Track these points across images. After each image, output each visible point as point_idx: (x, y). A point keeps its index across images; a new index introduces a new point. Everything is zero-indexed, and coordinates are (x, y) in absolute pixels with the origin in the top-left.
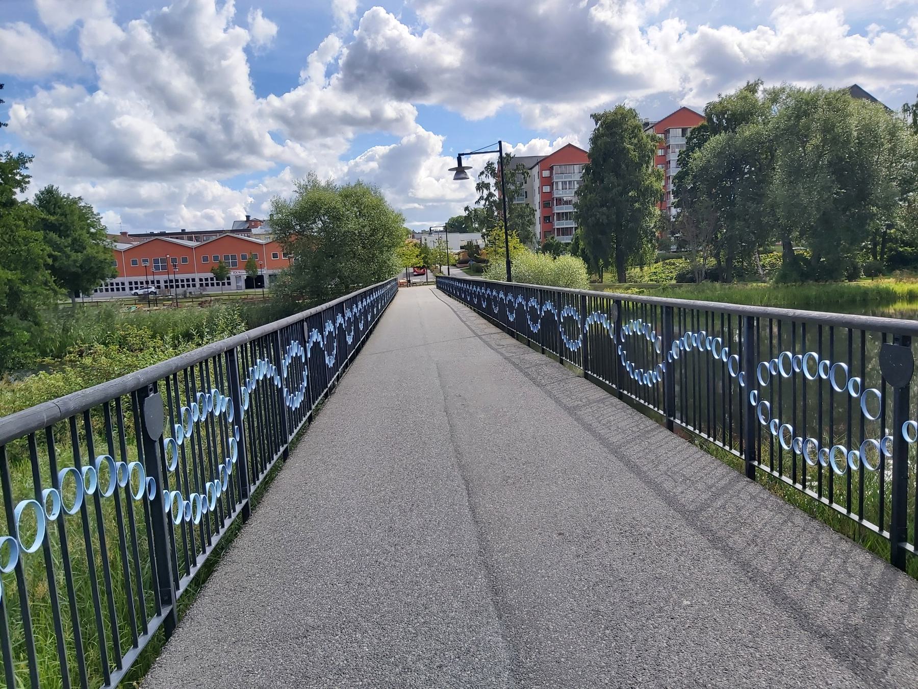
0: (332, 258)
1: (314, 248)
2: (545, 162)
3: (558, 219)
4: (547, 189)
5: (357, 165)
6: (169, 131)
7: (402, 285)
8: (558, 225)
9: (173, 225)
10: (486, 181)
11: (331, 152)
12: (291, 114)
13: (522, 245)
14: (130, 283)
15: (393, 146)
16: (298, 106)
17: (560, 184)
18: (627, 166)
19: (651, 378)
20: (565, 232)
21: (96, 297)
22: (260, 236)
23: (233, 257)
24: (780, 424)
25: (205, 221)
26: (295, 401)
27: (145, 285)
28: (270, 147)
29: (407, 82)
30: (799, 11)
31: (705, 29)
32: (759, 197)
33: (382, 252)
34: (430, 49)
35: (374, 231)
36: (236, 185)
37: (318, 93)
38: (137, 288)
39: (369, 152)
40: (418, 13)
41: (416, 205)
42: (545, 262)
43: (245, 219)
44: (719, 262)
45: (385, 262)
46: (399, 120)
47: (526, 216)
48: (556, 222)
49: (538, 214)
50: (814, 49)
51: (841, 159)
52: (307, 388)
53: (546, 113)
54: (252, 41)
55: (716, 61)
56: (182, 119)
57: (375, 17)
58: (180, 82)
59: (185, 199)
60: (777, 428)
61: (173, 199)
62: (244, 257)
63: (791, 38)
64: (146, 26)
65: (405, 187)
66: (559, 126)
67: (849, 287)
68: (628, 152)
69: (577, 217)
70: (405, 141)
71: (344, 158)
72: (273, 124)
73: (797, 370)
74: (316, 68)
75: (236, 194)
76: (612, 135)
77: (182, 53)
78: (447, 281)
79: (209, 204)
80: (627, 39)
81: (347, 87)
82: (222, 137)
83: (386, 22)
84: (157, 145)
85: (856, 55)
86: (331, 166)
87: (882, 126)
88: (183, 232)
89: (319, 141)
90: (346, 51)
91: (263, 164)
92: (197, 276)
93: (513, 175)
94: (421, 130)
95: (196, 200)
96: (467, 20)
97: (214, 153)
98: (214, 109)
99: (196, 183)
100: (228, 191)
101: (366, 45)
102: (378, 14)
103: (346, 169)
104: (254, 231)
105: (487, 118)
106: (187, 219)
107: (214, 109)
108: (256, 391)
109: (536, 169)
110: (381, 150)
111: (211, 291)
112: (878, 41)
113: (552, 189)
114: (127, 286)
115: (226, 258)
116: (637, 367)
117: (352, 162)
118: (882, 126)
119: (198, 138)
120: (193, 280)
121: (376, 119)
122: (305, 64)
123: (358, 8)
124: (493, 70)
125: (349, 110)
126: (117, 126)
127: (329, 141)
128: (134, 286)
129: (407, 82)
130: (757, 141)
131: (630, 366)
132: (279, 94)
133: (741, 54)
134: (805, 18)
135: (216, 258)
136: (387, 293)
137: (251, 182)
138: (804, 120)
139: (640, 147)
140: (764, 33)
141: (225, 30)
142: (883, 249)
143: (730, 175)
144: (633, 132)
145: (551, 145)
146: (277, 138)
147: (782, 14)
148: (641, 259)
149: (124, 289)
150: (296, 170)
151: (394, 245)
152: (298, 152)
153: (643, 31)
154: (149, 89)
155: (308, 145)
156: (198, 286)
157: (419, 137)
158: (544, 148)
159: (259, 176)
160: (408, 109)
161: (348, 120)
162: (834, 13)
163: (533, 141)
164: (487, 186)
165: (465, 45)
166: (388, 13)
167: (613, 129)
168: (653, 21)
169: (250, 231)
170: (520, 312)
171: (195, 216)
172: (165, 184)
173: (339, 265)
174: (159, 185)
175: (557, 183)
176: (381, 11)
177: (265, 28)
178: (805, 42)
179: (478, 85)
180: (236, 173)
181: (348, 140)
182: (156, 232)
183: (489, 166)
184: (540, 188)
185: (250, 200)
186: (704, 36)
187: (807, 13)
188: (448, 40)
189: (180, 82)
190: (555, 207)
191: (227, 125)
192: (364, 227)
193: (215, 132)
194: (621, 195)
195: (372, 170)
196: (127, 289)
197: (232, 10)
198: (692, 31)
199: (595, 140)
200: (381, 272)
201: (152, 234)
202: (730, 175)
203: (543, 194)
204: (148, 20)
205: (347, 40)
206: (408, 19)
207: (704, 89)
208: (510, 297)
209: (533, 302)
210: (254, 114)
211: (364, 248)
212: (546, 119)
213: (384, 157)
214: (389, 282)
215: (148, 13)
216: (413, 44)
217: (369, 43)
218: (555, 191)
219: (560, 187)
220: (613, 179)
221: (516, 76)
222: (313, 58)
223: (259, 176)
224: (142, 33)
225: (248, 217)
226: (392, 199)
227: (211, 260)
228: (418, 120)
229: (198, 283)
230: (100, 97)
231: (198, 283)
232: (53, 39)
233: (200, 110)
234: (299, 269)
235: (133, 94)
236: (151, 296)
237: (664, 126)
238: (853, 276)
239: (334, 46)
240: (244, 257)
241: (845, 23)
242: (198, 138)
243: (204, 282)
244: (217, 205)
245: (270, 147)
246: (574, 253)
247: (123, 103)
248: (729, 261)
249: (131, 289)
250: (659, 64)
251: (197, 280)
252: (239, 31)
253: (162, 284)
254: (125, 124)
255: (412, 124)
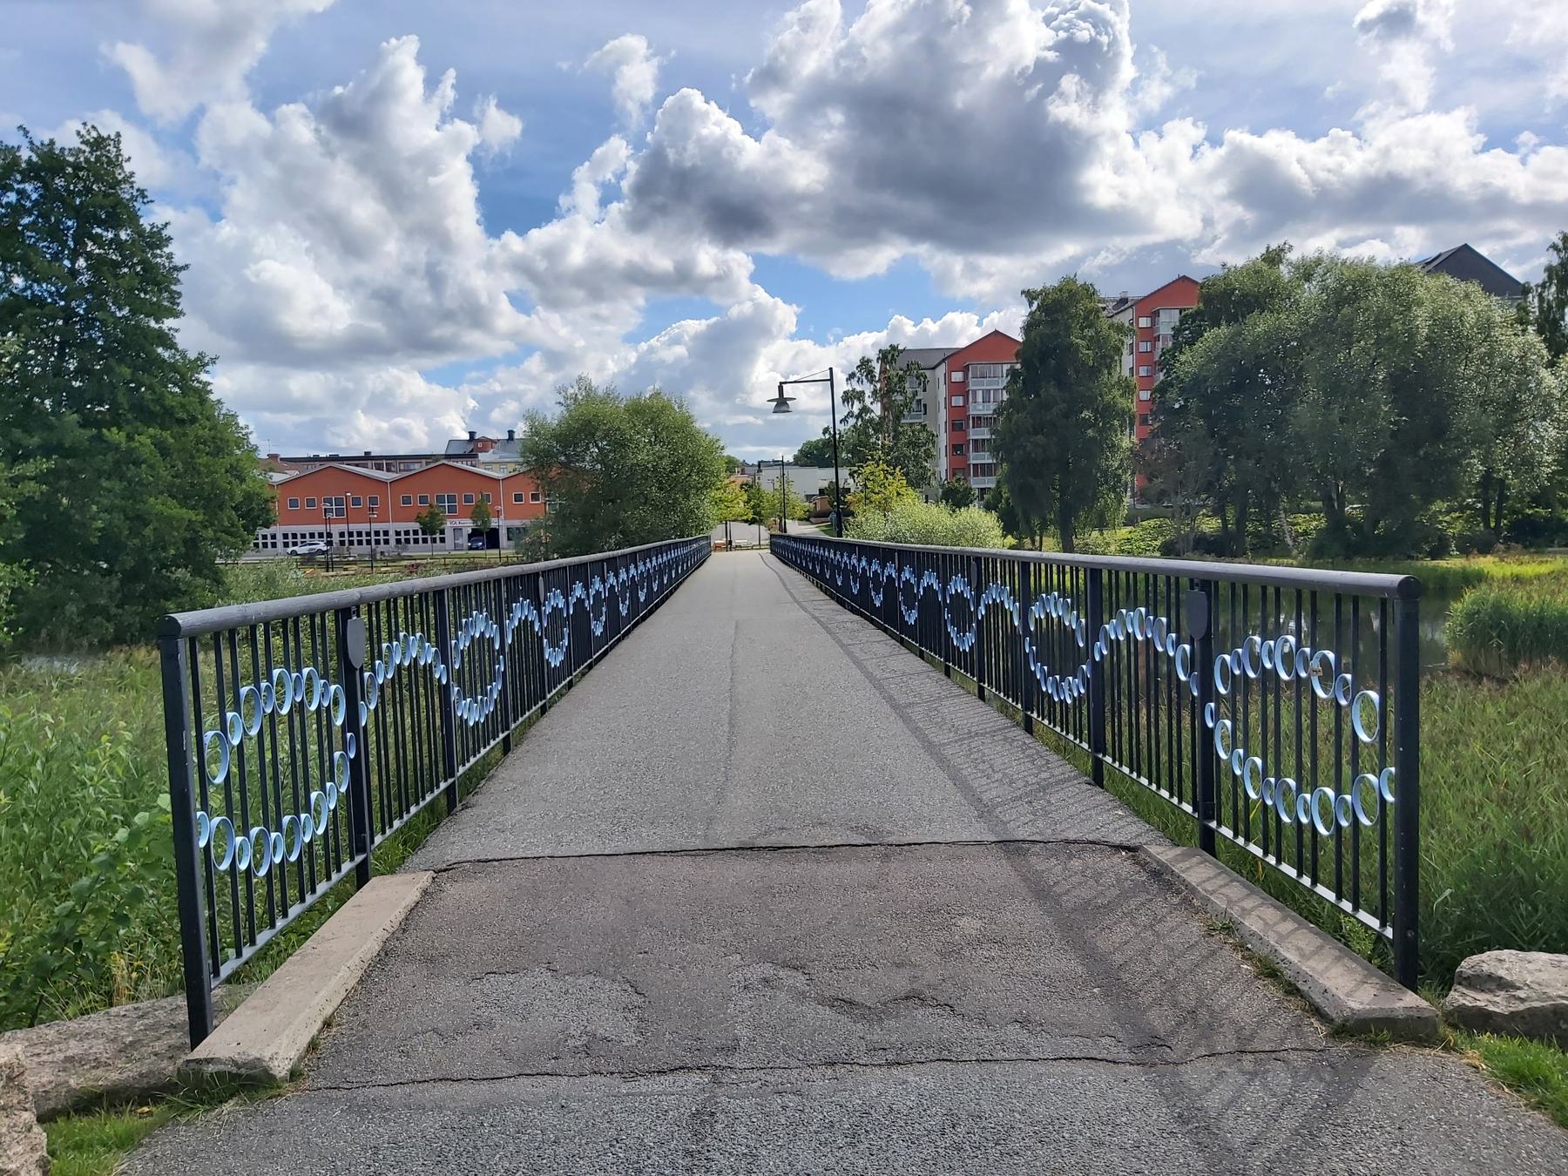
0: (611, 504)
1: (586, 487)
2: (957, 359)
3: (976, 450)
4: (958, 401)
5: (651, 350)
6: (337, 286)
7: (718, 548)
8: (975, 458)
9: (342, 443)
10: (859, 389)
11: (611, 328)
12: (542, 265)
13: (910, 491)
14: (286, 536)
15: (714, 319)
16: (553, 253)
17: (980, 394)
18: (1077, 372)
19: (1072, 689)
20: (984, 470)
21: (248, 558)
22: (493, 465)
23: (452, 499)
24: (1247, 755)
25: (395, 438)
26: (554, 657)
27: (308, 539)
28: (506, 317)
29: (737, 214)
30: (1403, 113)
31: (1238, 136)
32: (1279, 425)
33: (687, 497)
34: (772, 163)
35: (677, 465)
36: (448, 378)
37: (586, 232)
38: (295, 544)
39: (675, 329)
40: (752, 103)
41: (751, 419)
42: (937, 517)
43: (467, 437)
44: (1225, 522)
45: (692, 512)
46: (723, 278)
47: (921, 444)
48: (972, 454)
49: (943, 440)
50: (1428, 173)
51: (1406, 371)
52: (568, 647)
53: (973, 272)
54: (483, 141)
55: (1264, 192)
56: (362, 269)
57: (684, 110)
58: (365, 211)
59: (364, 400)
60: (1242, 762)
61: (344, 399)
62: (468, 499)
63: (1386, 153)
64: (305, 117)
65: (731, 389)
66: (979, 298)
67: (1435, 569)
68: (1077, 350)
69: (995, 450)
70: (734, 312)
71: (632, 339)
72: (511, 281)
73: (1160, 649)
74: (586, 193)
75: (449, 393)
76: (1054, 322)
77: (363, 165)
78: (818, 551)
79: (402, 411)
80: (1109, 149)
81: (637, 224)
82: (428, 299)
83: (704, 116)
84: (321, 311)
85: (1499, 182)
86: (608, 356)
87: (1471, 318)
88: (367, 456)
89: (587, 310)
90: (633, 167)
91: (495, 347)
92: (392, 527)
93: (901, 379)
94: (761, 294)
95: (382, 403)
96: (837, 117)
97: (414, 327)
98: (420, 254)
99: (383, 374)
100: (437, 391)
101: (666, 157)
102: (690, 104)
103: (633, 357)
104: (482, 457)
105: (874, 277)
106: (364, 433)
107: (420, 254)
108: (518, 628)
109: (942, 369)
110: (694, 326)
111: (414, 550)
112: (1534, 160)
113: (966, 401)
114: (280, 540)
115: (440, 499)
116: (1051, 673)
117: (644, 346)
118: (1471, 318)
119: (388, 299)
120: (386, 533)
121: (683, 276)
122: (568, 185)
123: (656, 95)
124: (888, 199)
125: (636, 258)
126: (253, 279)
127: (604, 309)
128: (290, 540)
129: (737, 214)
130: (1275, 337)
131: (1042, 670)
132: (522, 232)
133: (1304, 178)
134: (1409, 122)
135: (423, 500)
136: (686, 557)
137: (474, 374)
138: (1346, 310)
139: (1097, 342)
140: (1343, 141)
141: (438, 129)
142: (1499, 509)
143: (1238, 388)
144: (1086, 318)
145: (980, 324)
146: (520, 303)
147: (1372, 116)
148: (1101, 516)
149: (274, 545)
150: (555, 359)
151: (706, 486)
152: (552, 327)
153: (1134, 135)
154: (312, 220)
155: (570, 316)
156: (393, 542)
157: (757, 306)
158: (965, 330)
159: (488, 365)
160: (739, 260)
161: (637, 276)
162: (1460, 114)
163: (950, 316)
164: (860, 396)
165: (836, 157)
166: (707, 102)
167: (1060, 309)
168: (1151, 123)
169: (476, 456)
170: (890, 587)
171: (378, 429)
172: (330, 376)
173: (622, 514)
174: (321, 377)
175: (975, 392)
176: (697, 98)
177: (503, 127)
178: (1411, 161)
179: (856, 224)
180: (451, 358)
181: (638, 309)
182: (323, 455)
183: (865, 364)
184: (948, 400)
185: (472, 404)
186: (1237, 151)
187: (1414, 114)
188: (804, 147)
189: (365, 211)
190: (971, 430)
191: (435, 279)
192: (661, 458)
193: (418, 292)
194: (1066, 416)
195: (679, 360)
196: (280, 545)
197: (450, 94)
198: (1214, 141)
199: (1028, 328)
200: (689, 524)
201: (316, 459)
202: (1238, 388)
203: (951, 409)
204: (310, 107)
205: (637, 144)
206: (739, 110)
207: (1240, 234)
208: (875, 567)
209: (891, 570)
210: (481, 263)
211: (661, 489)
212: (973, 280)
213: (697, 337)
214: (696, 540)
215: (310, 95)
216: (750, 153)
217: (671, 154)
218: (971, 405)
219: (980, 399)
220: (1053, 391)
221: (924, 209)
222: (582, 173)
223: (488, 365)
224: (300, 127)
225: (472, 434)
226: (706, 412)
227: (415, 501)
228: (754, 278)
229: (392, 538)
230: (226, 231)
231: (392, 538)
232: (157, 136)
233: (393, 253)
234: (562, 518)
235: (282, 228)
236: (320, 558)
237: (1150, 305)
238: (1439, 552)
239: (618, 155)
240: (468, 499)
241: (1479, 131)
242: (388, 299)
243: (403, 537)
244: (415, 412)
245: (506, 317)
246: (988, 508)
247: (264, 242)
248: (1241, 520)
249: (286, 545)
250: (1157, 195)
251: (392, 533)
252: (461, 126)
253: (336, 539)
254: (266, 276)
255: (745, 284)
